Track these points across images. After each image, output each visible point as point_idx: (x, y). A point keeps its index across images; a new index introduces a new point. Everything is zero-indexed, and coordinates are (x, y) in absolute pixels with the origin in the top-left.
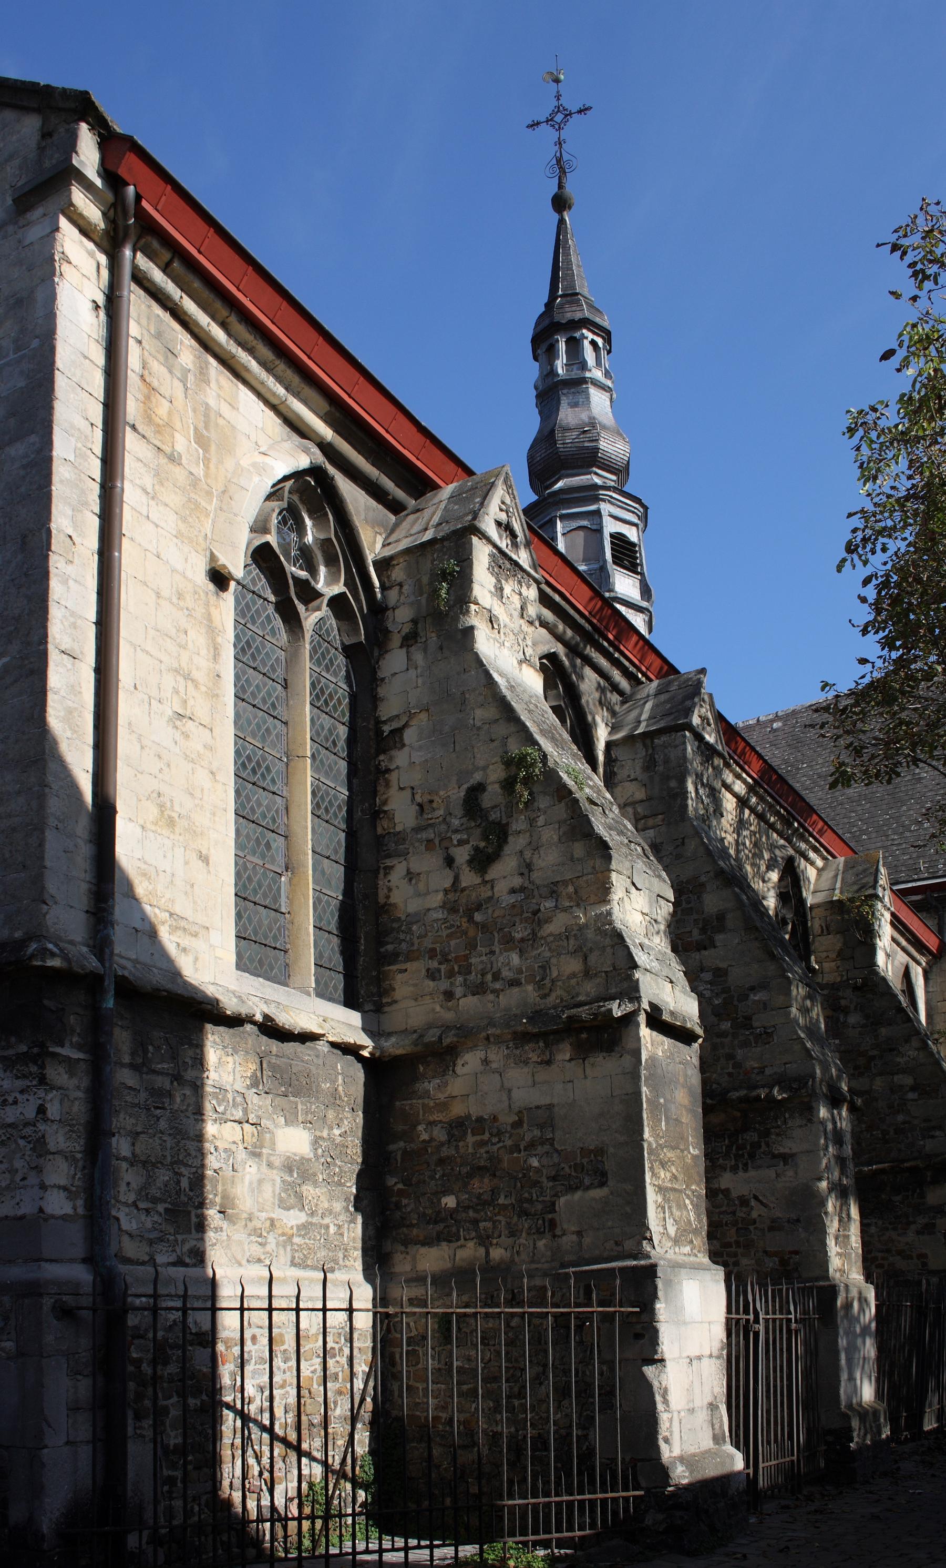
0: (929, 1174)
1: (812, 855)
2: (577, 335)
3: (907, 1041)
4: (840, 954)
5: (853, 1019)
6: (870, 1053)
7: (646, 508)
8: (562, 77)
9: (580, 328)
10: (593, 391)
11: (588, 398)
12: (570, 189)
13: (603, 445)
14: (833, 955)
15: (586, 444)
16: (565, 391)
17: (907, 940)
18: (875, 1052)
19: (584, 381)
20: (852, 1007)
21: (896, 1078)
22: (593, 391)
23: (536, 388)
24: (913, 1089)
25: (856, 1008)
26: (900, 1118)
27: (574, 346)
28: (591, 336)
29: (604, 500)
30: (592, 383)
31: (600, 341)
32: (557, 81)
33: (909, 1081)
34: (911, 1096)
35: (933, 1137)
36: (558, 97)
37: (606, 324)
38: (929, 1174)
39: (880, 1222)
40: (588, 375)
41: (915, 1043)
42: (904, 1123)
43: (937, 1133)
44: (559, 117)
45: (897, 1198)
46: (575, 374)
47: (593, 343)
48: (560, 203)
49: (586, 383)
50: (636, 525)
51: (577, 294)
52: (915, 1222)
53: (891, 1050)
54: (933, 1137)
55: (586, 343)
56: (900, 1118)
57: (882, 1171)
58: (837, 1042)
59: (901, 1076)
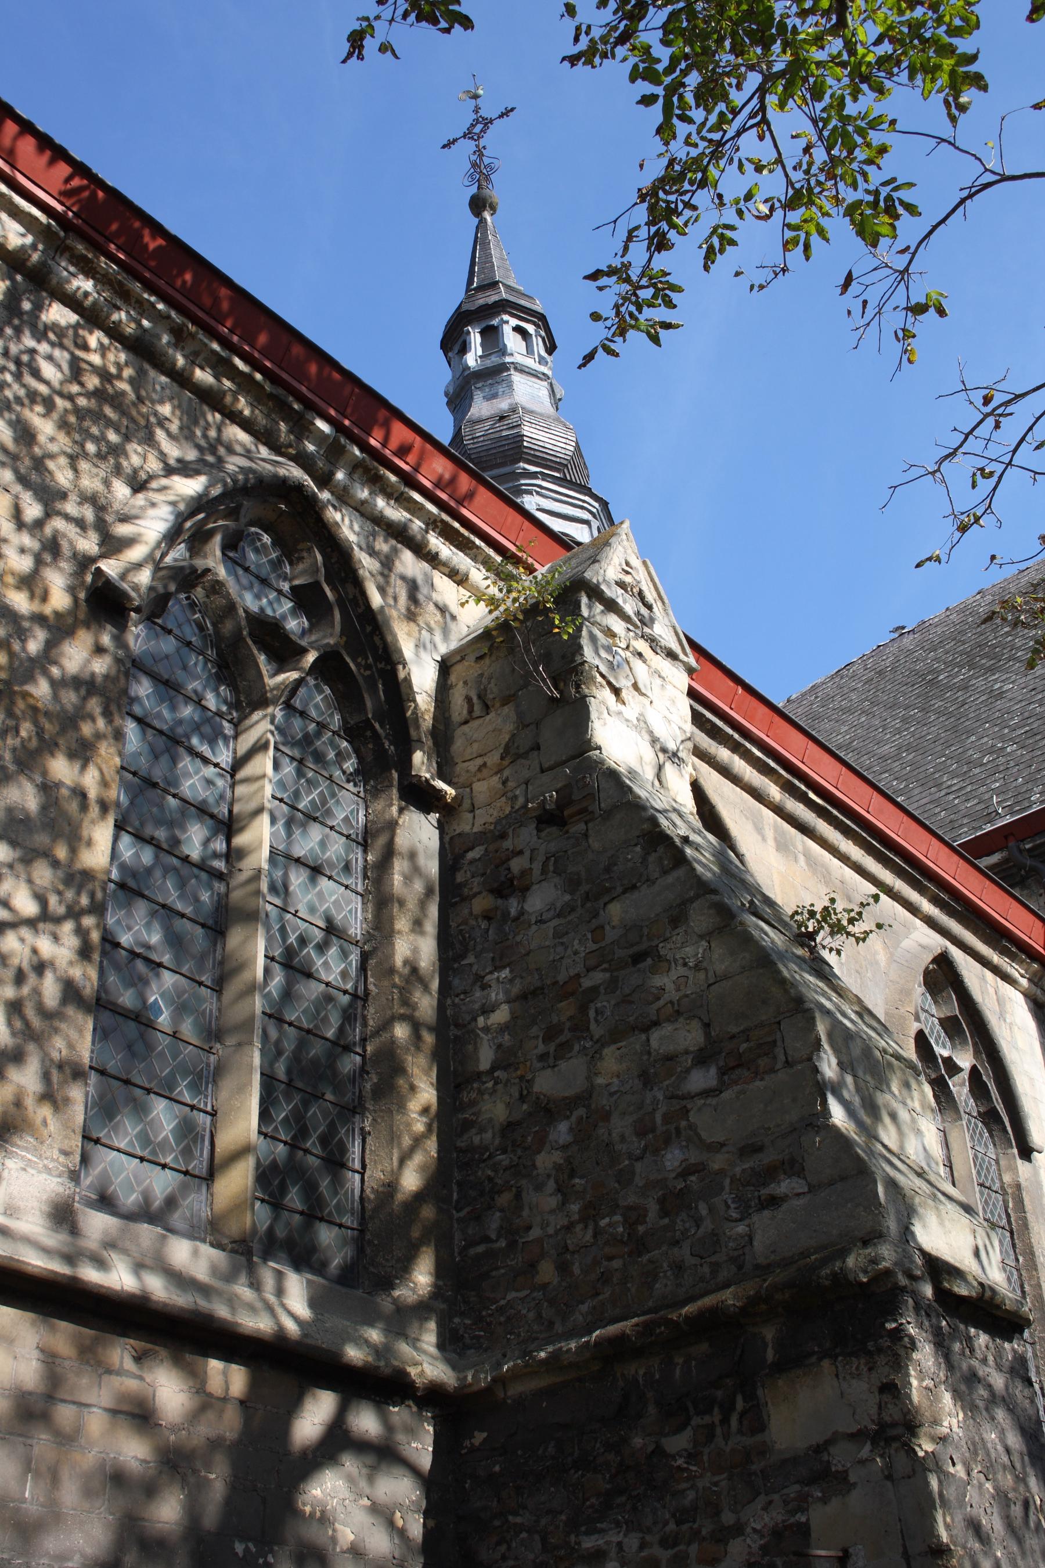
0: (769, 1333)
1: (435, 542)
2: (495, 322)
3: (677, 917)
4: (512, 753)
5: (537, 902)
6: (587, 983)
7: (604, 504)
8: (481, 92)
9: (498, 314)
10: (517, 378)
11: (510, 385)
12: (496, 192)
13: (527, 430)
14: (493, 759)
15: (504, 433)
16: (479, 385)
17: (935, 901)
18: (599, 977)
19: (503, 368)
20: (537, 867)
21: (655, 1036)
22: (517, 378)
23: (446, 394)
24: (702, 1059)
25: (544, 871)
26: (673, 1158)
27: (491, 334)
28: (514, 322)
29: (530, 493)
30: (516, 369)
31: (531, 328)
32: (476, 97)
33: (688, 1036)
34: (700, 1079)
35: (774, 1202)
36: (476, 110)
37: (538, 307)
38: (769, 1333)
39: (632, 1542)
40: (508, 359)
41: (700, 919)
42: (685, 1173)
43: (785, 1186)
44: (479, 126)
45: (678, 1443)
46: (494, 360)
47: (518, 329)
48: (479, 205)
49: (508, 369)
50: (587, 522)
51: (497, 283)
52: (738, 1530)
53: (637, 959)
54: (774, 1202)
55: (507, 330)
56: (673, 1158)
57: (616, 1350)
58: (505, 973)
59: (667, 1029)
